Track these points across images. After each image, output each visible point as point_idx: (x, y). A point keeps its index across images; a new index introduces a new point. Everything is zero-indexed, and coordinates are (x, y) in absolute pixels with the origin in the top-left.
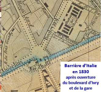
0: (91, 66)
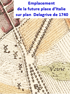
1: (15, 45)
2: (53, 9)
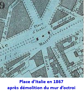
0: (40, 82)
1: (37, 38)
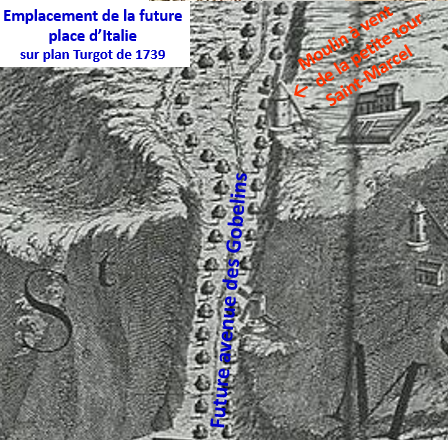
2: (94, 37)
